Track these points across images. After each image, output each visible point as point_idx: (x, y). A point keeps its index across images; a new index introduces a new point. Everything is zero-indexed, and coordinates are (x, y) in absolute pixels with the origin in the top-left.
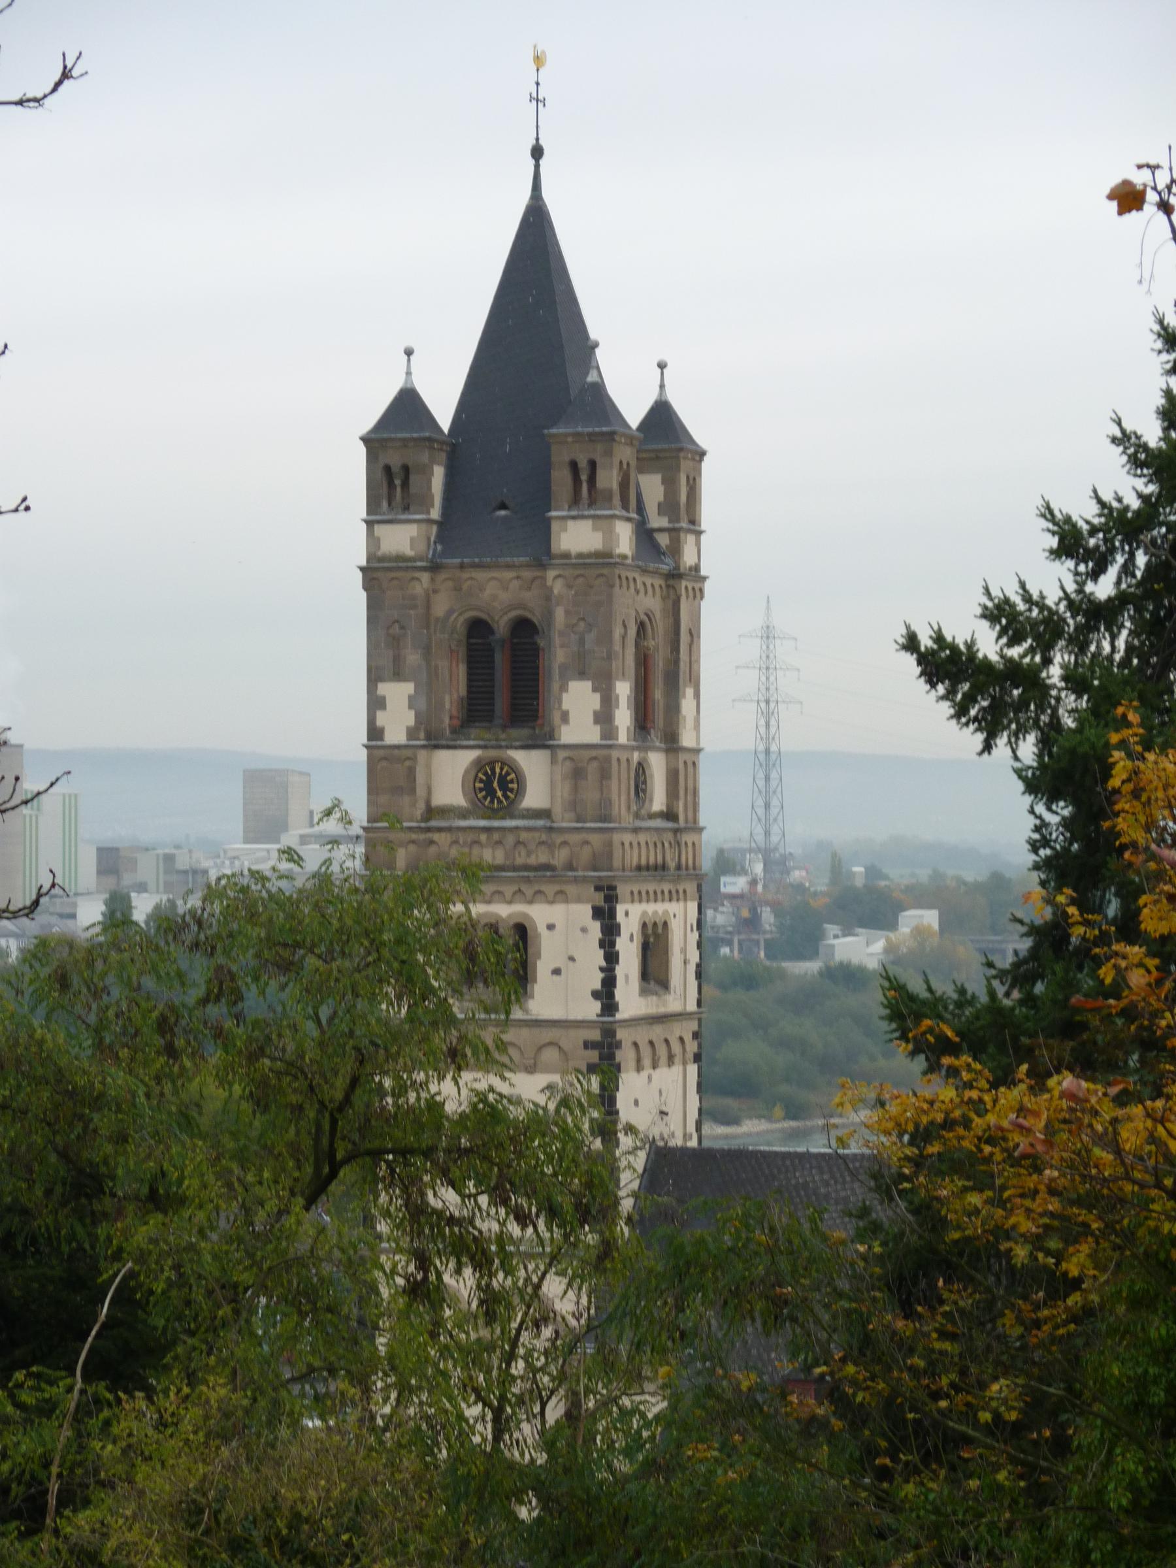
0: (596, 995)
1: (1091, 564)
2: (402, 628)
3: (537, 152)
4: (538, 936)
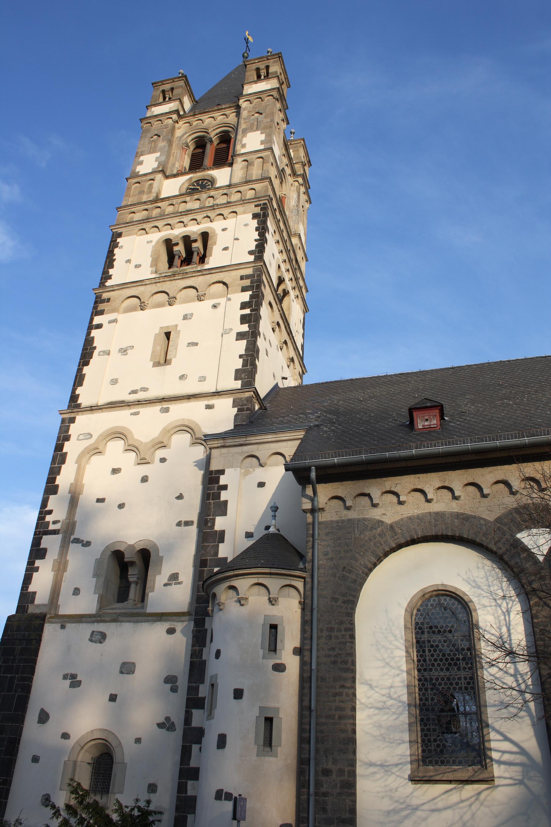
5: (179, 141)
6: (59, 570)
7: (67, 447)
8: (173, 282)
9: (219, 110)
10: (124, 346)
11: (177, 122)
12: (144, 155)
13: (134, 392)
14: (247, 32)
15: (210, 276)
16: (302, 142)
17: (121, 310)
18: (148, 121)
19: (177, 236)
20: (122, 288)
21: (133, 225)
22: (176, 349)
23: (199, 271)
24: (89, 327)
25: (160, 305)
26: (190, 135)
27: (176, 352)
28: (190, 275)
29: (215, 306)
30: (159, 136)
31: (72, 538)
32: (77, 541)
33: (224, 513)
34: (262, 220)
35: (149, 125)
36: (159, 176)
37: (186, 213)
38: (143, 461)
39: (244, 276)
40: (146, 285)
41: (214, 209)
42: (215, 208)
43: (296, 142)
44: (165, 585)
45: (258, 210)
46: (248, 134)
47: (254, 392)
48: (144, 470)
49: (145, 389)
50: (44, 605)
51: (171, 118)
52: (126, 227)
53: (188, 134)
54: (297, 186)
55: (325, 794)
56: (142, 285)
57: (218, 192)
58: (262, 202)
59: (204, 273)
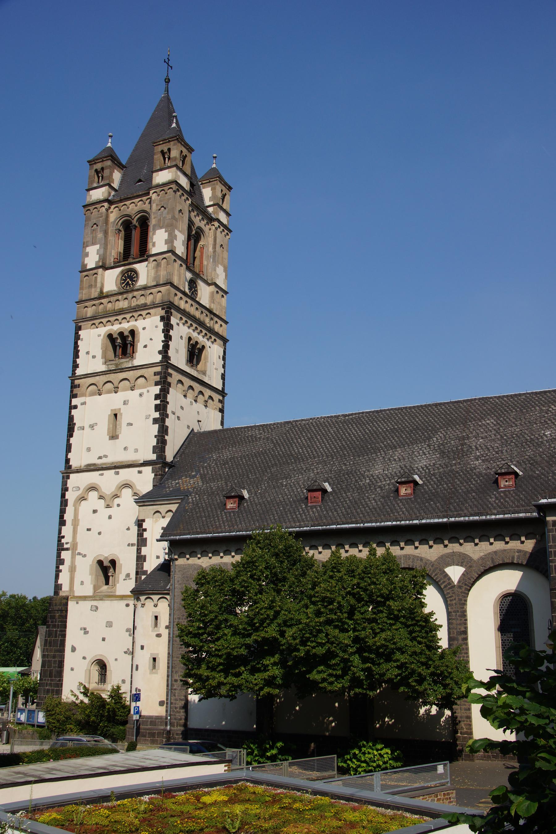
0: (160, 352)
1: (422, 711)
2: (97, 226)
3: (167, 81)
4: (139, 333)
6: (72, 571)
7: (68, 495)
10: (92, 423)
13: (100, 458)
17: (88, 393)
22: (121, 427)
25: (109, 392)
31: (77, 552)
32: (79, 554)
33: (146, 545)
38: (108, 506)
44: (124, 580)
46: (157, 231)
48: (109, 511)
49: (106, 456)
50: (67, 591)
51: (104, 206)
55: (175, 689)
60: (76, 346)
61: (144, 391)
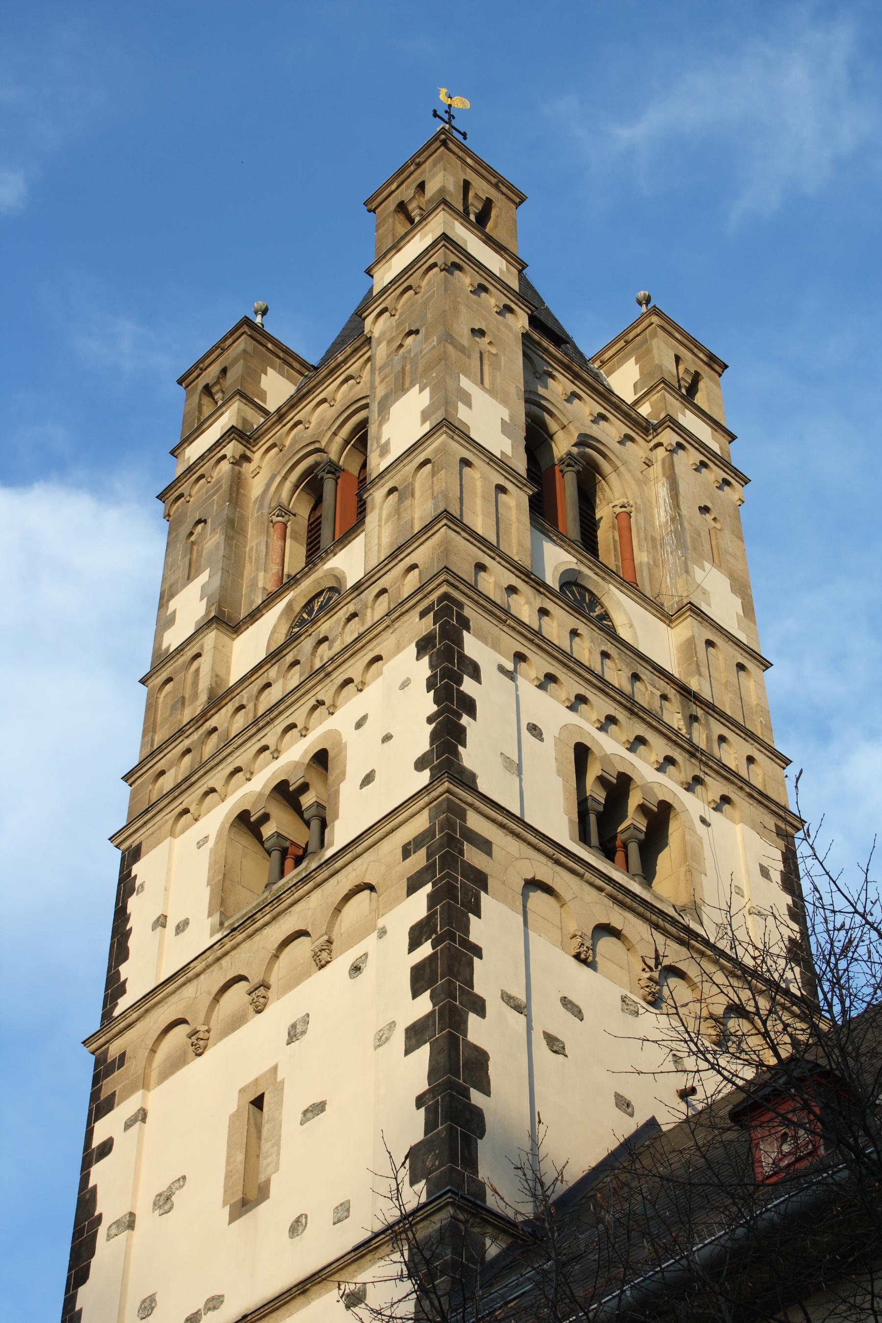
5: (261, 507)
8: (257, 938)
9: (332, 372)
11: (245, 458)
12: (177, 593)
14: (443, 92)
15: (333, 880)
16: (655, 319)
18: (177, 493)
19: (260, 794)
20: (147, 1011)
21: (161, 810)
22: (278, 1143)
23: (304, 880)
24: (84, 1159)
26: (285, 478)
27: (278, 1154)
28: (288, 901)
29: (356, 969)
30: (205, 521)
34: (439, 649)
35: (182, 502)
36: (211, 637)
37: (268, 719)
39: (409, 843)
40: (198, 975)
41: (328, 675)
42: (330, 669)
43: (638, 330)
45: (427, 625)
47: (452, 1204)
52: (145, 823)
53: (278, 479)
54: (663, 461)
56: (189, 980)
57: (335, 617)
58: (434, 596)
59: (319, 879)
60: (121, 915)
61: (370, 944)
